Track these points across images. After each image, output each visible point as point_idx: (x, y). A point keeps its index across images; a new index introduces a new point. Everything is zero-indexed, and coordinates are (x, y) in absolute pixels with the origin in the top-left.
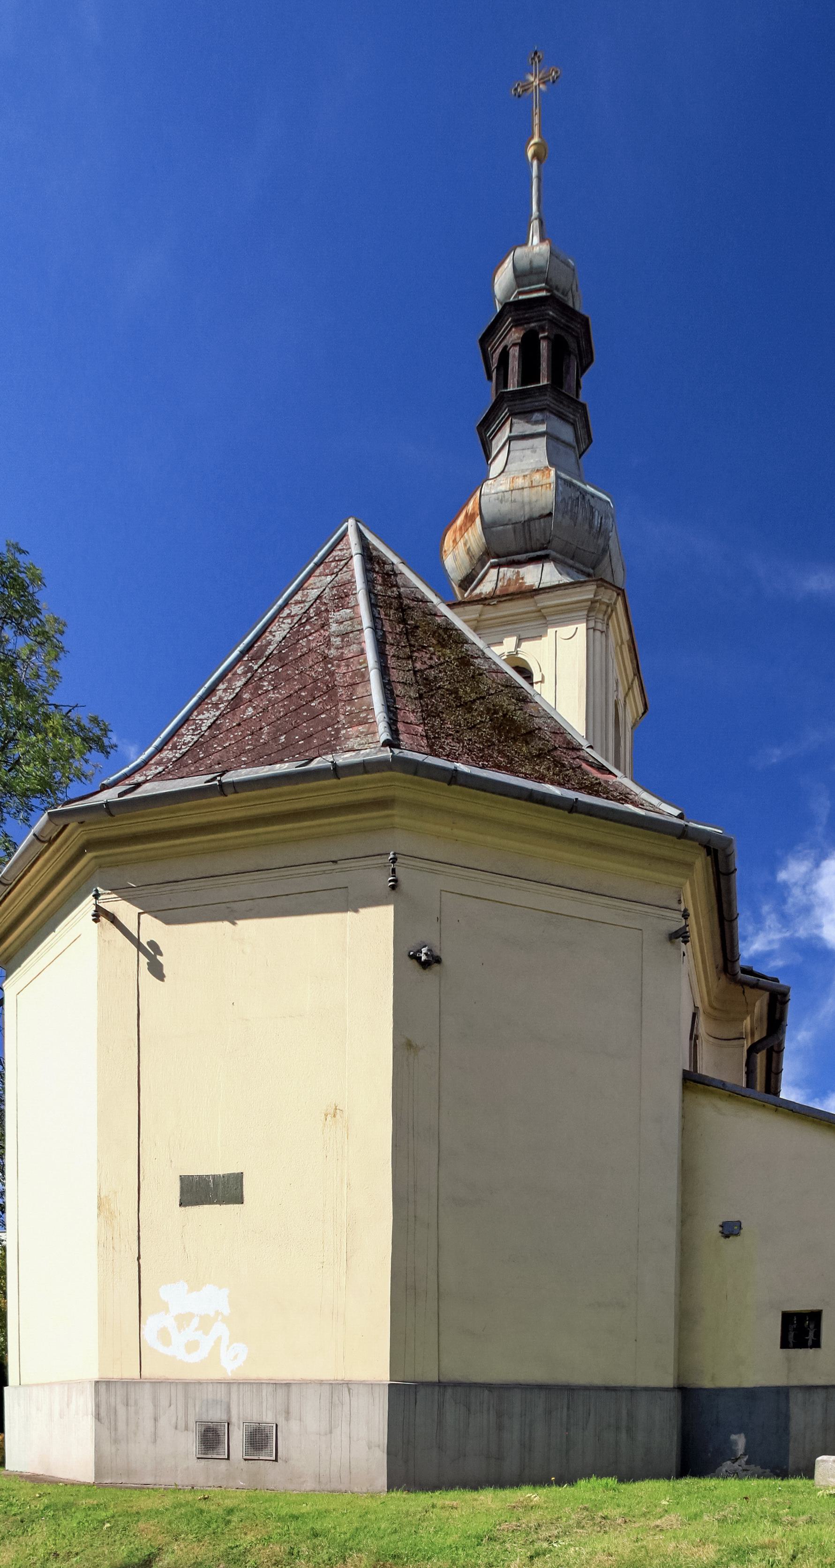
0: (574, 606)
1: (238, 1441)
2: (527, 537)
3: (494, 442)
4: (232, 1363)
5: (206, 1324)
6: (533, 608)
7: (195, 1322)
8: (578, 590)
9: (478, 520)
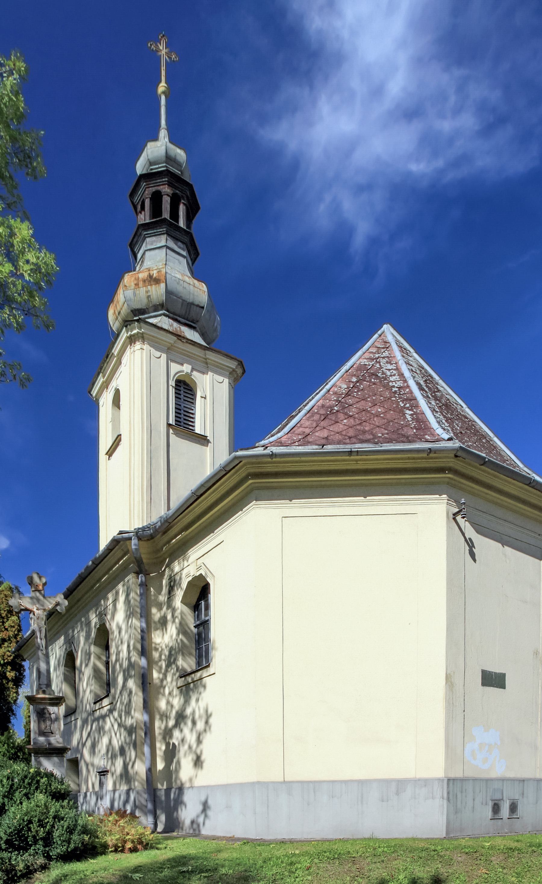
0: (227, 368)
1: (505, 811)
2: (187, 313)
3: (148, 240)
4: (498, 770)
6: (204, 356)
8: (229, 360)
9: (163, 285)
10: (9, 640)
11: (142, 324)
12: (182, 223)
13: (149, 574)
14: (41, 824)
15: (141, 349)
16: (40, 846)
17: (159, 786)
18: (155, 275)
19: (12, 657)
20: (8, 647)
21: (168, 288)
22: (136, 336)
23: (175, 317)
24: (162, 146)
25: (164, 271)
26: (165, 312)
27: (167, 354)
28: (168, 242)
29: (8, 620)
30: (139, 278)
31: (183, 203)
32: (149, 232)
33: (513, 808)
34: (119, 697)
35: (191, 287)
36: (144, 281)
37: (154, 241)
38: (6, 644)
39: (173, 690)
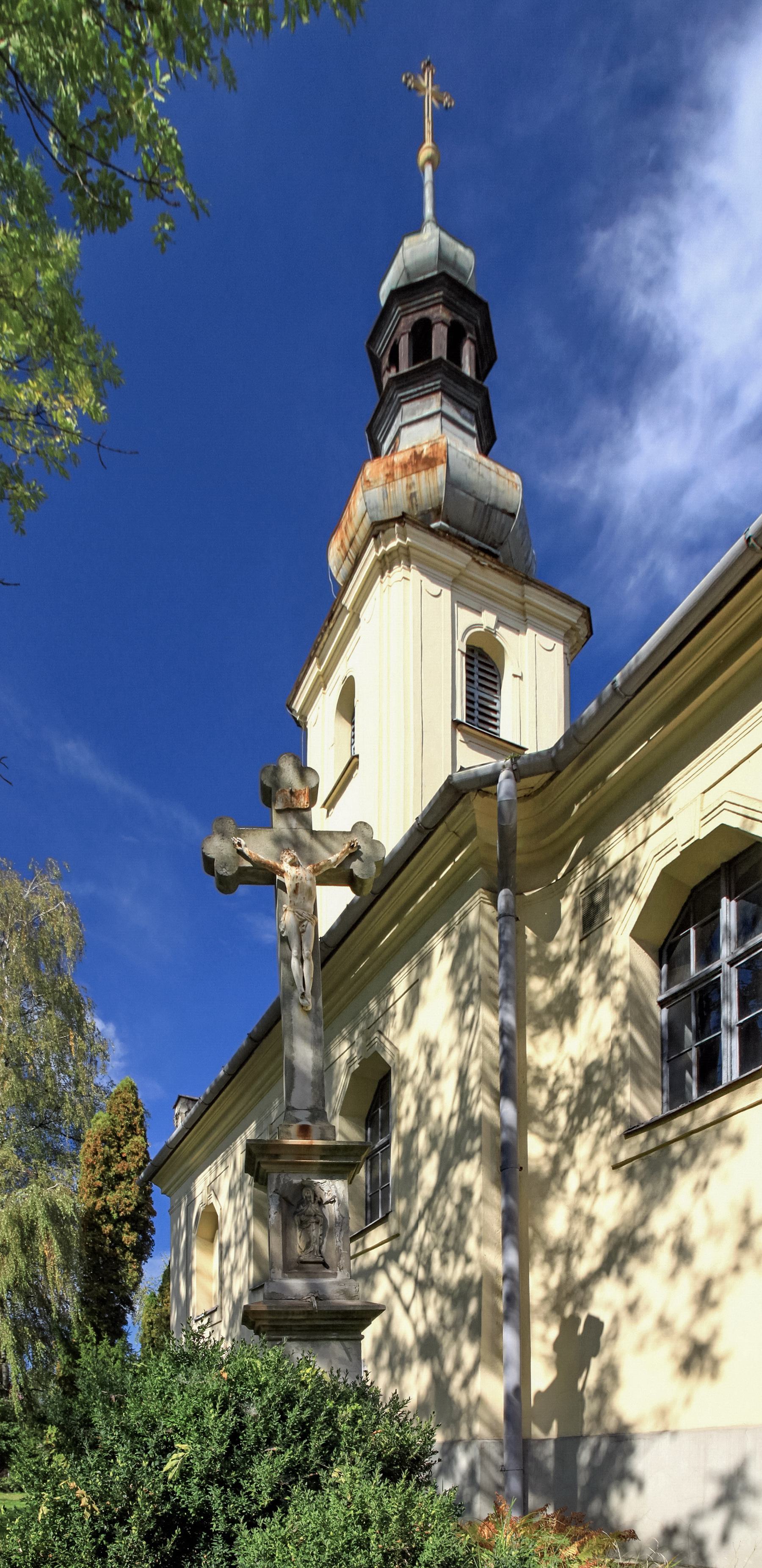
2: (485, 524)
3: (405, 407)
8: (565, 605)
9: (441, 469)
10: (129, 1176)
12: (467, 369)
13: (522, 894)
15: (404, 578)
17: (536, 1432)
18: (425, 453)
19: (132, 1208)
21: (451, 471)
22: (395, 554)
24: (430, 238)
26: (443, 524)
27: (451, 590)
29: (127, 1143)
30: (393, 463)
31: (470, 338)
32: (408, 392)
34: (421, 1216)
35: (493, 475)
36: (404, 466)
37: (418, 408)
38: (123, 1184)
39: (595, 1178)
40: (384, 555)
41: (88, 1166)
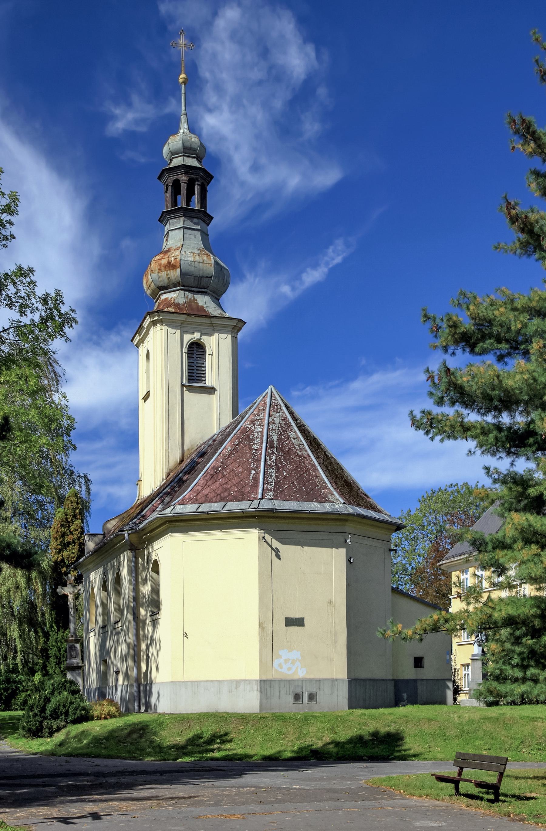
1: (305, 698)
3: (171, 221)
4: (301, 674)
5: (293, 662)
7: (290, 662)
9: (178, 270)
11: (160, 314)
14: (64, 706)
16: (63, 717)
20: (72, 549)
21: (182, 270)
23: (190, 288)
25: (178, 258)
28: (186, 222)
29: (73, 524)
33: (311, 697)
36: (165, 267)
40: (153, 321)
41: (54, 538)
